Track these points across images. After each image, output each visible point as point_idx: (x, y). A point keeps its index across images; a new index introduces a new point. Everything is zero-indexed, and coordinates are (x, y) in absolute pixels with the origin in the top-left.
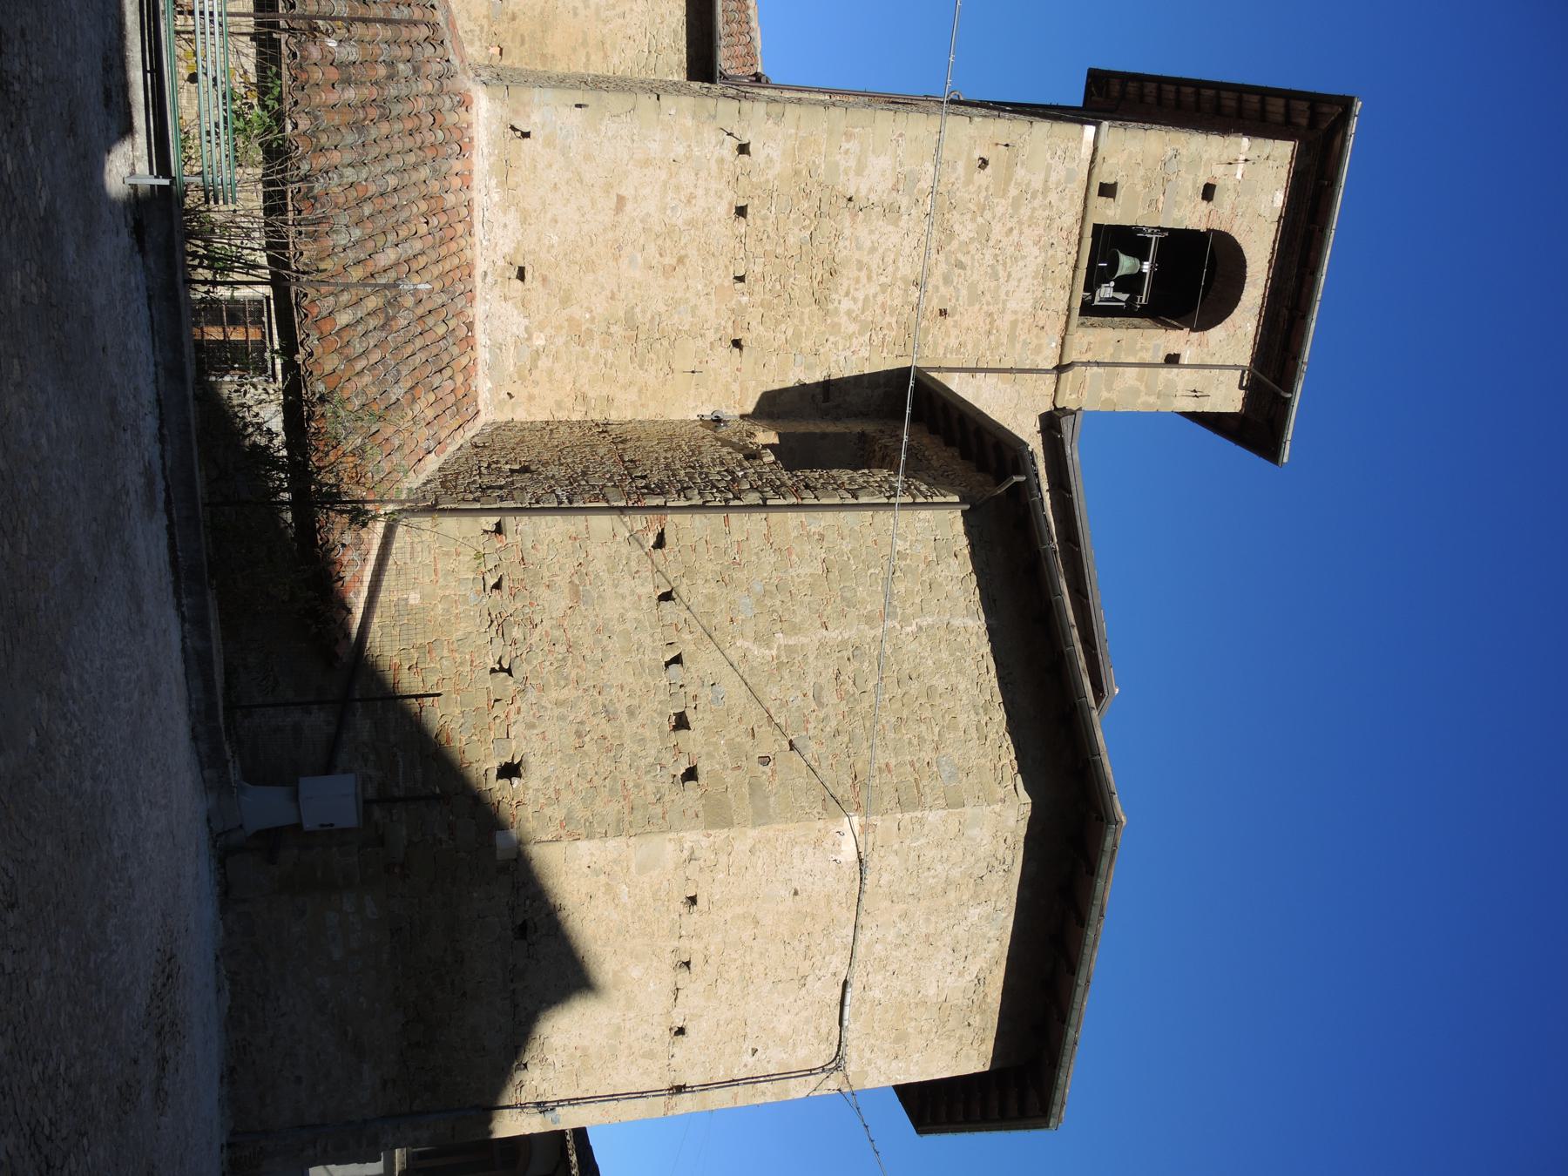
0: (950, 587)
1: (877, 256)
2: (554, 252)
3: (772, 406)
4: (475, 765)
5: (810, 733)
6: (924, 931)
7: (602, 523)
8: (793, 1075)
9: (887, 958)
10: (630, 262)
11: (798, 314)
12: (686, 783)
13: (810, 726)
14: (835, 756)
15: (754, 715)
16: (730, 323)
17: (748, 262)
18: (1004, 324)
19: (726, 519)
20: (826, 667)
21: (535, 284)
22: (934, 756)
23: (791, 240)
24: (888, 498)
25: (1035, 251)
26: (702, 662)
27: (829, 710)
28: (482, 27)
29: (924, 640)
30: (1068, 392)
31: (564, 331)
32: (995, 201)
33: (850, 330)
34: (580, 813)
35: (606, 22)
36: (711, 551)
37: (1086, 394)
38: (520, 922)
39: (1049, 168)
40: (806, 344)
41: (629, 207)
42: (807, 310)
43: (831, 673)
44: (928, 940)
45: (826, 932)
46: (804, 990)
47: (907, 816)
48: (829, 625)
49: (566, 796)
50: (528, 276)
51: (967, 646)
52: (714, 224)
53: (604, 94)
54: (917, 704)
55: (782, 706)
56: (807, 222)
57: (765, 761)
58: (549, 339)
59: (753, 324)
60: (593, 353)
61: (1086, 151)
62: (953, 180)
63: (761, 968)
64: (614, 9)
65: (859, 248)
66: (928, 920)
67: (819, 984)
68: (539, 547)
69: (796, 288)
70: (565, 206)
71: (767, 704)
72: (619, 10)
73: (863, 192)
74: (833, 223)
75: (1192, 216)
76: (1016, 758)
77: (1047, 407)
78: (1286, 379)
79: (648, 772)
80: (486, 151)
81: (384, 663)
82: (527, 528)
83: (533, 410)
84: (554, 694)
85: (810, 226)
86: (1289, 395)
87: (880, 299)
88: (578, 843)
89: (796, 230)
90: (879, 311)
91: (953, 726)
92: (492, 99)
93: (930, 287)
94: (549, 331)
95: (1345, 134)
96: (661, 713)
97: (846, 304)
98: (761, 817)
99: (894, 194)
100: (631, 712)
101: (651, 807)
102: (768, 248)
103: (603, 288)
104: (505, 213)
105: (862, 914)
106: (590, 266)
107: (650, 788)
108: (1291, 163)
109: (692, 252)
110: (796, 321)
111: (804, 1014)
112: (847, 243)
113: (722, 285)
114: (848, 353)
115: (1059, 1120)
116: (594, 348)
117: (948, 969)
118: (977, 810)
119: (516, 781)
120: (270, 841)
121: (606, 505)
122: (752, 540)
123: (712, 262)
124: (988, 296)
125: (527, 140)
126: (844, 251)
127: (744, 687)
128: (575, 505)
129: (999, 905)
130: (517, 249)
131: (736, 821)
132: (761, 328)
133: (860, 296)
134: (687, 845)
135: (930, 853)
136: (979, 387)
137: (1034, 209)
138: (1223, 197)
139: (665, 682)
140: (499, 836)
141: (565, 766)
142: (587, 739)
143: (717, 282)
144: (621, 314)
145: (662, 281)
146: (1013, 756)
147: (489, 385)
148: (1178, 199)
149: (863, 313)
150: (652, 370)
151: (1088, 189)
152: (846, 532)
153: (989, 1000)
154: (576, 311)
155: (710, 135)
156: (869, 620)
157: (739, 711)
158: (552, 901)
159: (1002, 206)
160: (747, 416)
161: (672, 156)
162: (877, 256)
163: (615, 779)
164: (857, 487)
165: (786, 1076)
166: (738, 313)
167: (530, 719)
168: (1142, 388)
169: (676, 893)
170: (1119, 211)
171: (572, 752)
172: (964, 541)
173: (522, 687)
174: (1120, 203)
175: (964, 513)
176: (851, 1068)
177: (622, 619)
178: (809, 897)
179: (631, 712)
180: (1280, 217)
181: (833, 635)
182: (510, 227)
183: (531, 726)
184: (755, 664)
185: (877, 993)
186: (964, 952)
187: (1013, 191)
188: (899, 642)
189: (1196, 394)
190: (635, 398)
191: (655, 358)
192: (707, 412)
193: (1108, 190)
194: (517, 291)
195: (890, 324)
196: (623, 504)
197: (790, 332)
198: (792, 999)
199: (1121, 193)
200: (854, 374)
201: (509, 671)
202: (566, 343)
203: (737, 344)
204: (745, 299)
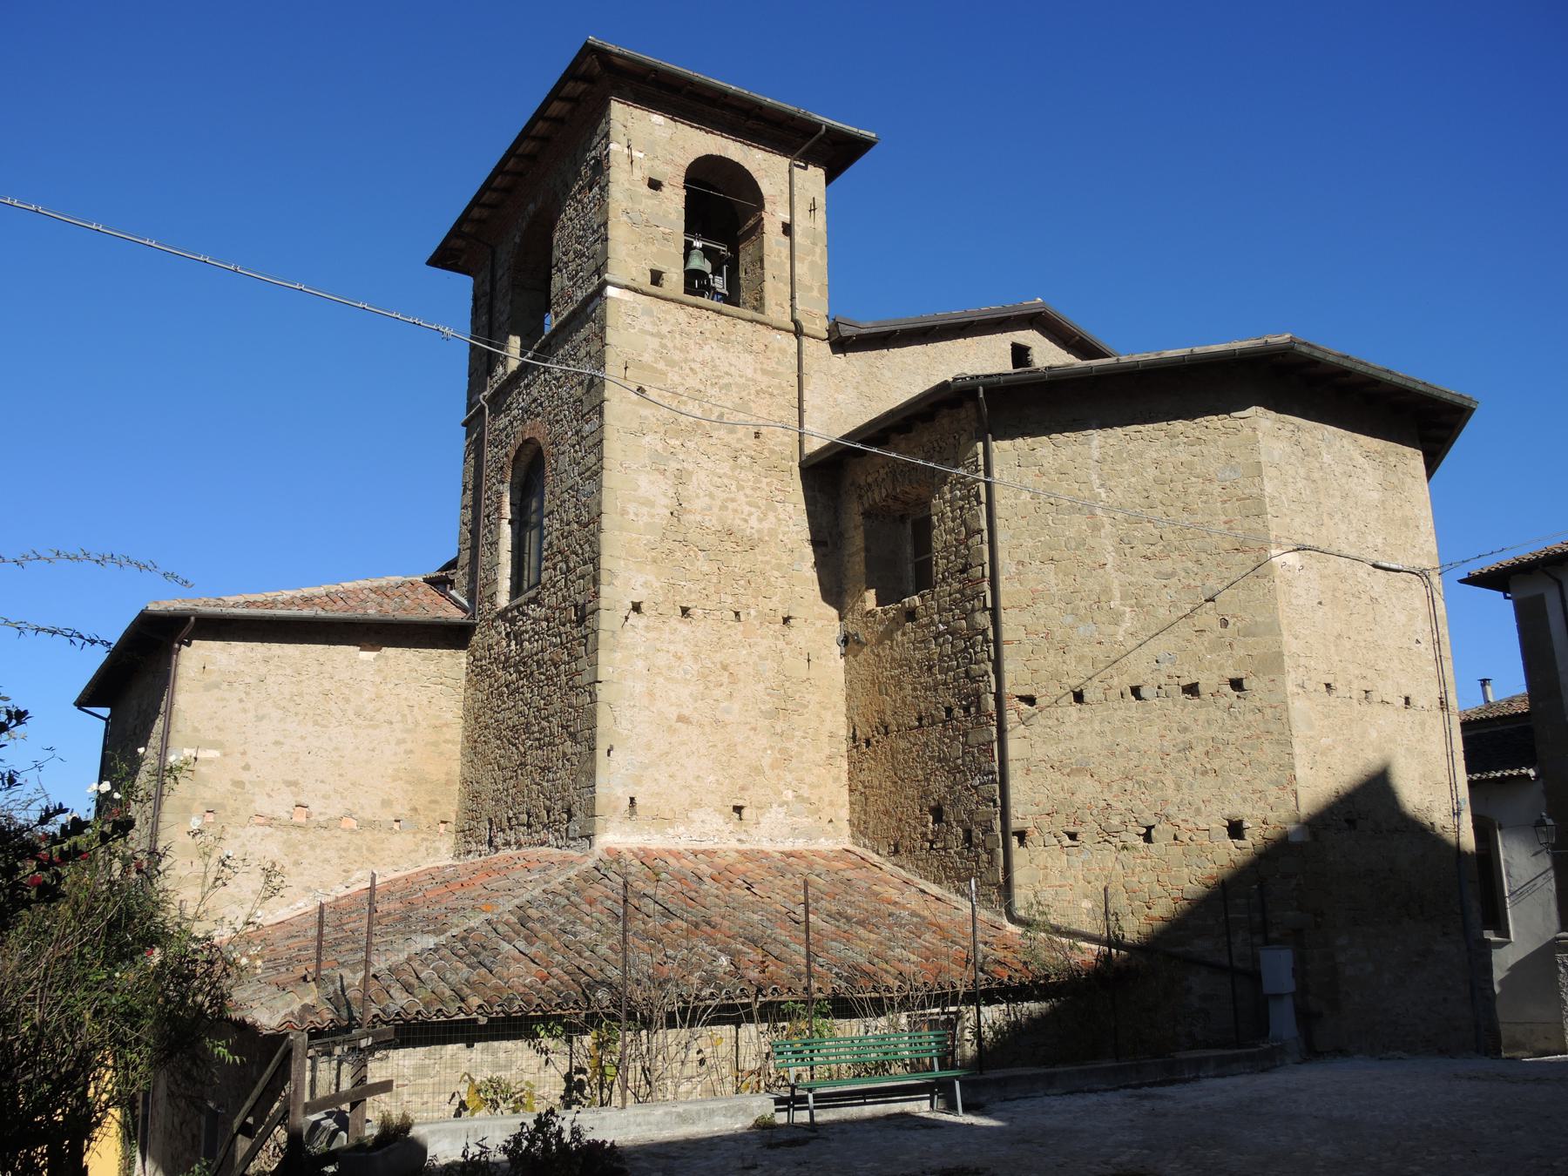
0: (1064, 457)
1: (718, 493)
2: (721, 779)
3: (834, 591)
4: (1233, 857)
5: (1199, 584)
6: (1339, 500)
7: (1014, 747)
8: (1432, 611)
9: (1357, 531)
10: (728, 713)
11: (762, 566)
12: (1245, 688)
13: (1193, 583)
14: (1218, 565)
15: (1185, 629)
16: (771, 626)
17: (724, 607)
18: (764, 381)
19: (1008, 642)
20: (1139, 567)
21: (746, 797)
22: (1216, 484)
23: (705, 569)
24: (980, 503)
25: (707, 348)
26: (1138, 669)
27: (1179, 567)
28: (423, 839)
29: (1113, 484)
30: (814, 326)
31: (781, 773)
32: (669, 382)
33: (774, 520)
34: (1272, 774)
35: (417, 724)
36: (1037, 657)
37: (816, 311)
38: (1346, 825)
39: (643, 331)
40: (785, 559)
41: (686, 712)
42: (760, 558)
43: (1144, 563)
44: (1345, 497)
45: (1343, 580)
46: (1379, 600)
47: (1269, 510)
48: (1102, 562)
49: (1258, 785)
50: (740, 803)
51: (1117, 448)
52: (696, 637)
53: (599, 730)
54: (1171, 493)
55: (1176, 606)
56: (691, 553)
57: (1225, 623)
58: (788, 785)
59: (771, 606)
60: (796, 748)
61: (628, 296)
62: (654, 419)
63: (1367, 633)
64: (405, 715)
65: (710, 508)
66: (1333, 496)
67: (1375, 587)
68: (1037, 801)
69: (743, 566)
70: (686, 769)
71: (1174, 618)
72: (406, 711)
73: (666, 501)
74: (691, 531)
75: (674, 201)
76: (1217, 415)
77: (826, 346)
78: (809, 128)
79: (1236, 718)
80: (646, 837)
81: (1146, 929)
82: (1020, 810)
83: (840, 802)
84: (1170, 792)
85: (694, 551)
86: (824, 127)
87: (749, 491)
88: (1297, 776)
89: (699, 563)
90: (758, 493)
91: (1190, 466)
92: (605, 830)
93: (739, 446)
94: (781, 787)
95: (618, 55)
96: (1185, 706)
97: (753, 522)
98: (1274, 629)
99: (667, 473)
100: (1185, 730)
101: (1266, 717)
102: (712, 590)
103: (748, 737)
104: (693, 822)
105: (1331, 550)
106: (731, 747)
107: (1250, 717)
108: (629, 105)
109: (718, 657)
110: (768, 567)
111: (1394, 600)
112: (707, 518)
113: (744, 631)
114: (791, 522)
115: (1470, 399)
116: (792, 746)
117: (1361, 481)
118: (1262, 452)
119: (1246, 824)
120: (1305, 1018)
121: (996, 745)
122: (1026, 623)
123: (726, 640)
124: (744, 394)
125: (637, 800)
126: (712, 522)
127: (1160, 636)
128: (997, 769)
129: (1320, 437)
130: (721, 812)
131: (1277, 649)
132: (774, 599)
133: (747, 509)
134: (1296, 690)
135: (1291, 493)
136: (813, 406)
137: (675, 347)
138: (662, 171)
139: (1156, 701)
140: (1293, 839)
141: (1233, 785)
142: (1208, 766)
143: (740, 637)
144: (767, 722)
145: (741, 685)
146: (1215, 418)
147: (823, 840)
148: (661, 214)
149: (760, 508)
150: (808, 697)
151: (657, 297)
152: (1015, 542)
153: (1379, 449)
154: (766, 762)
155: (628, 637)
156: (1096, 528)
157: (1180, 641)
158: (1333, 799)
159: (673, 377)
160: (840, 614)
161: (645, 672)
162: (718, 493)
163: (1243, 745)
164: (963, 529)
165: (1434, 617)
166: (764, 619)
167: (1192, 812)
168: (810, 258)
169: (1326, 700)
170: (673, 269)
171: (1220, 779)
172: (1019, 441)
173: (1164, 818)
174: (666, 267)
175: (995, 439)
176: (1425, 563)
177: (1101, 734)
178: (1322, 592)
179: (1185, 730)
180: (672, 119)
181: (1110, 559)
182: (704, 817)
183: (1198, 811)
184: (1139, 625)
185: (1379, 541)
186: (1351, 467)
187: (661, 365)
188: (1115, 504)
189: (813, 209)
190: (829, 713)
191: (799, 694)
192: (837, 650)
193: (656, 277)
194: (751, 813)
195: (767, 484)
196: (994, 730)
197: (777, 574)
198: (1385, 610)
199: (659, 267)
200: (806, 518)
201: (1149, 828)
202: (790, 771)
203: (786, 620)
204: (753, 612)
